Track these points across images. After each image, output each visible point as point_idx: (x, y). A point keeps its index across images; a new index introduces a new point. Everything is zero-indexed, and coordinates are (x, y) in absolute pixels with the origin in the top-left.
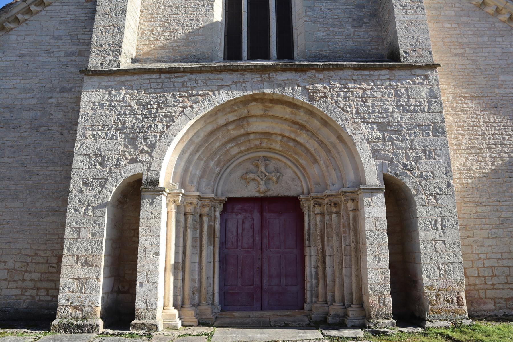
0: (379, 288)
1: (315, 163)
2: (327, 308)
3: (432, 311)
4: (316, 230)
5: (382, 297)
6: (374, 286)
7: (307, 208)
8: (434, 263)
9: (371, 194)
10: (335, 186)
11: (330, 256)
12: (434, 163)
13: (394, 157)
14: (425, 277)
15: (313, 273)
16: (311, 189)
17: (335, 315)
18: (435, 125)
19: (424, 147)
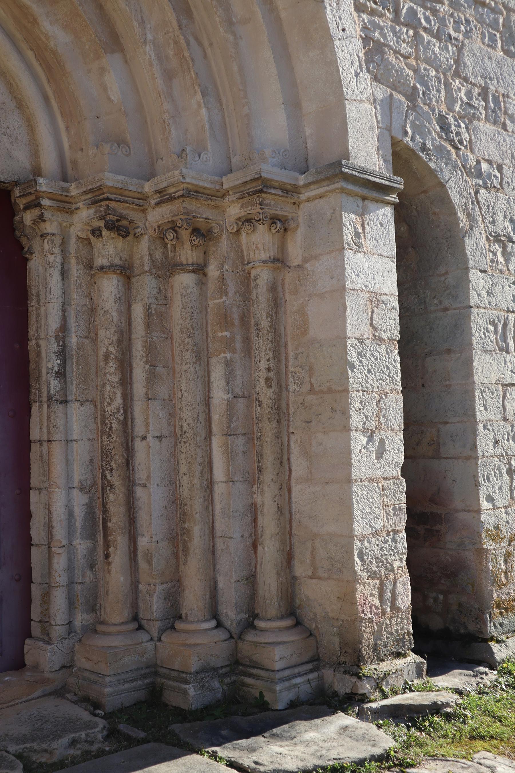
0: (382, 549)
1: (113, 52)
2: (150, 646)
3: (498, 606)
4: (94, 339)
5: (388, 579)
6: (369, 542)
7: (58, 240)
8: (502, 456)
9: (360, 202)
10: (203, 157)
11: (160, 438)
12: (504, 140)
13: (418, 86)
14: (485, 503)
15: (79, 512)
16: (75, 163)
17: (203, 670)
18: (508, 15)
19: (484, 77)
